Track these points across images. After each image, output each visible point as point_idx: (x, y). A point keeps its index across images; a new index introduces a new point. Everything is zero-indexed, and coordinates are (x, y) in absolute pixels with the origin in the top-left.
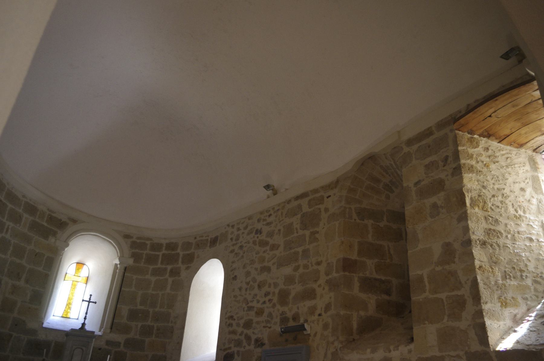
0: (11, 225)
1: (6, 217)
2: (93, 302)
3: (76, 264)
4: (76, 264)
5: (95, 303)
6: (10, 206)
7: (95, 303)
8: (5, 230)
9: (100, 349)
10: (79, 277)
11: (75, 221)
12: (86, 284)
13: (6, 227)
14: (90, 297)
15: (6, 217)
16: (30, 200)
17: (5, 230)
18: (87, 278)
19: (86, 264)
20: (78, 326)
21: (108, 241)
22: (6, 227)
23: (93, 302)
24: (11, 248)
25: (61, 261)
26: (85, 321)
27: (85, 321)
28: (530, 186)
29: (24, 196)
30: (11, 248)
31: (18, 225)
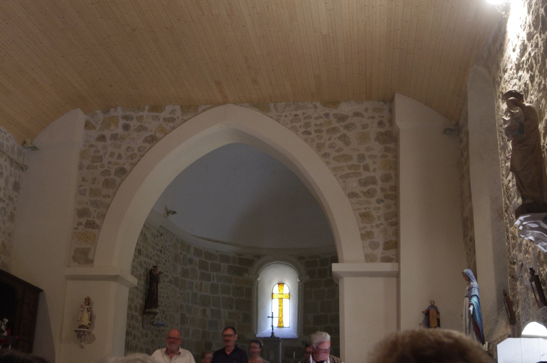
0: (215, 273)
1: (210, 270)
2: (270, 317)
3: (278, 285)
4: (277, 285)
5: (268, 317)
6: (210, 262)
7: (268, 317)
8: (212, 279)
9: (299, 348)
10: (290, 295)
11: (259, 257)
12: (289, 299)
13: (212, 276)
14: (273, 314)
15: (210, 270)
16: (222, 252)
17: (212, 279)
18: (273, 298)
19: (285, 283)
20: (270, 335)
21: (266, 266)
22: (212, 276)
23: (270, 317)
24: (220, 289)
25: (257, 287)
26: (273, 331)
27: (273, 331)
28: (523, 78)
29: (217, 251)
30: (220, 289)
31: (220, 272)
